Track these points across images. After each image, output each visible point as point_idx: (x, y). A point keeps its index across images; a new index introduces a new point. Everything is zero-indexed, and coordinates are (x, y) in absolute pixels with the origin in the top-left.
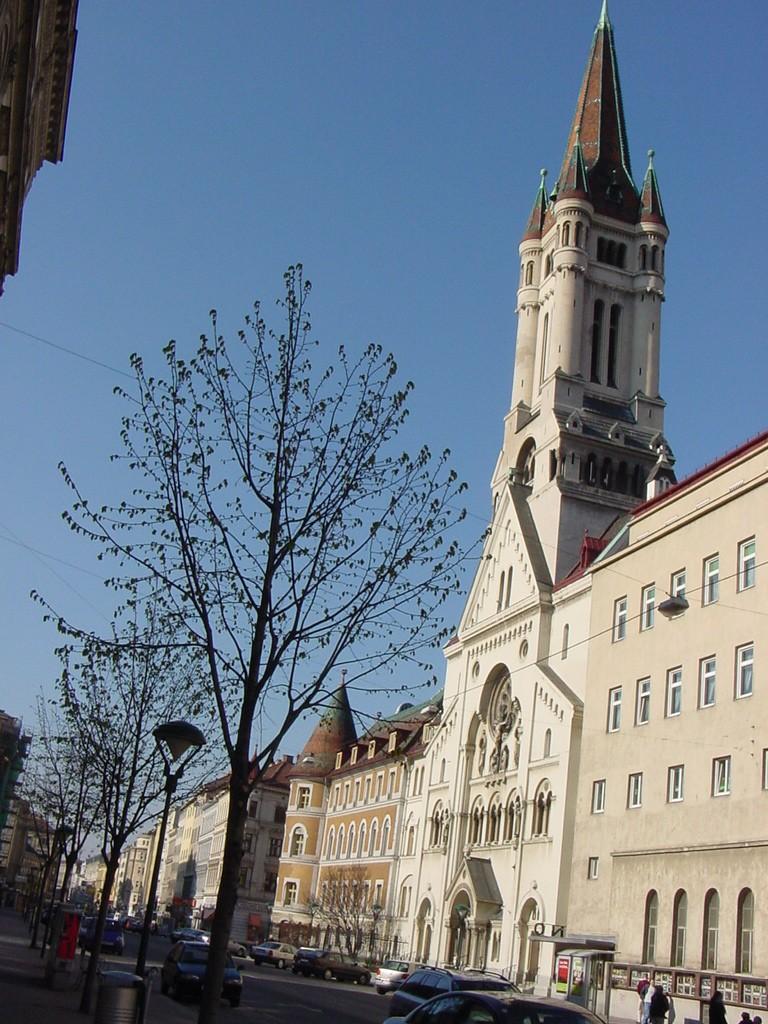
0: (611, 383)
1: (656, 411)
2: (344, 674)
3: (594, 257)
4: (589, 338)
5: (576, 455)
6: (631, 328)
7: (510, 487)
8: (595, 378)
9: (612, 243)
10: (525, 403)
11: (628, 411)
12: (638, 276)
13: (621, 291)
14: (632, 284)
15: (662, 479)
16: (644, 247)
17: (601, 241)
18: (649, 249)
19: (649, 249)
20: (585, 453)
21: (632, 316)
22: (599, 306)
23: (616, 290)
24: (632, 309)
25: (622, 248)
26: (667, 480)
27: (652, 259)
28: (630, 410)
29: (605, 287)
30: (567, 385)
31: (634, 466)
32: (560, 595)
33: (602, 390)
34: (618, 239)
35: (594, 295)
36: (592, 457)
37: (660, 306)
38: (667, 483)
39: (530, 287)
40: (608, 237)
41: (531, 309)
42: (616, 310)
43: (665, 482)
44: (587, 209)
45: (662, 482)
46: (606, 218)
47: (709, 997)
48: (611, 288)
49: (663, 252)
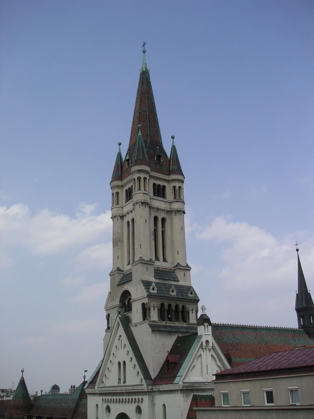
0: (165, 260)
1: (187, 273)
2: (23, 372)
3: (152, 194)
4: (153, 237)
5: (155, 306)
6: (172, 229)
7: (120, 318)
8: (157, 259)
9: (159, 185)
10: (120, 268)
11: (173, 274)
12: (172, 202)
13: (165, 210)
14: (170, 206)
15: (205, 324)
16: (174, 187)
17: (154, 185)
18: (177, 188)
19: (177, 188)
20: (159, 304)
21: (172, 223)
22: (156, 219)
23: (163, 210)
24: (172, 220)
25: (164, 187)
26: (207, 324)
27: (178, 192)
28: (174, 273)
29: (158, 209)
30: (146, 266)
31: (181, 306)
32: (159, 388)
33: (160, 264)
34: (162, 183)
35: (154, 214)
36: (162, 305)
37: (184, 215)
38: (207, 325)
39: (117, 206)
40: (158, 182)
41: (119, 218)
42: (164, 220)
43: (206, 325)
44: (148, 170)
45: (205, 325)
46: (156, 173)
47: (121, 309)
48: (161, 209)
49: (183, 188)
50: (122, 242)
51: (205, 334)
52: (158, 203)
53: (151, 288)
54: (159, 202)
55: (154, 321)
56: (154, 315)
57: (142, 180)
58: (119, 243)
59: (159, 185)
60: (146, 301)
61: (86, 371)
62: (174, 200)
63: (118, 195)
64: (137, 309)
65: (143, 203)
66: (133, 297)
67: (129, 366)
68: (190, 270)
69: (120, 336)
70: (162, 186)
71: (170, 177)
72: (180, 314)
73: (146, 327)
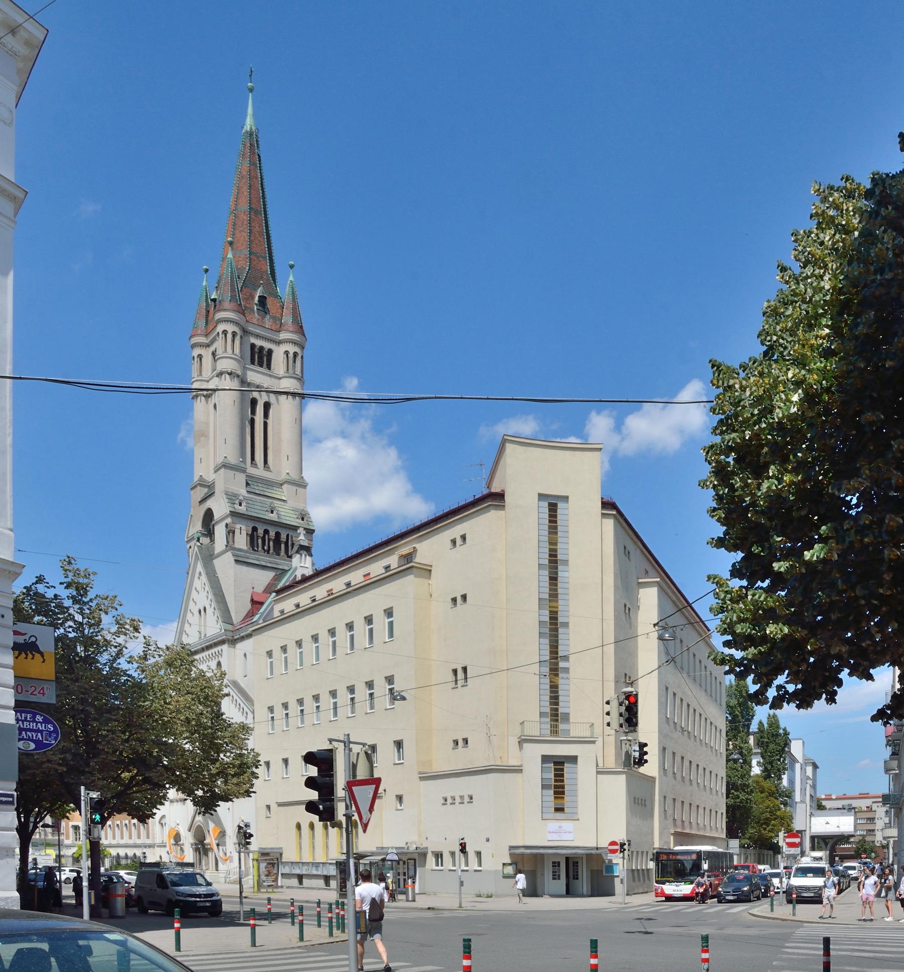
25: (270, 352)
34: (267, 345)
40: (259, 343)
42: (267, 406)
50: (207, 437)
51: (301, 565)
52: (255, 376)
53: (237, 502)
54: (260, 375)
55: (240, 550)
56: (241, 541)
57: (229, 336)
58: (202, 439)
59: (261, 348)
60: (229, 520)
61: (400, 798)
62: (287, 375)
63: (201, 359)
64: (220, 531)
65: (230, 374)
66: (216, 516)
67: (210, 610)
68: (892, 755)
69: (200, 572)
70: (266, 350)
71: (281, 335)
72: (283, 546)
73: (229, 557)
